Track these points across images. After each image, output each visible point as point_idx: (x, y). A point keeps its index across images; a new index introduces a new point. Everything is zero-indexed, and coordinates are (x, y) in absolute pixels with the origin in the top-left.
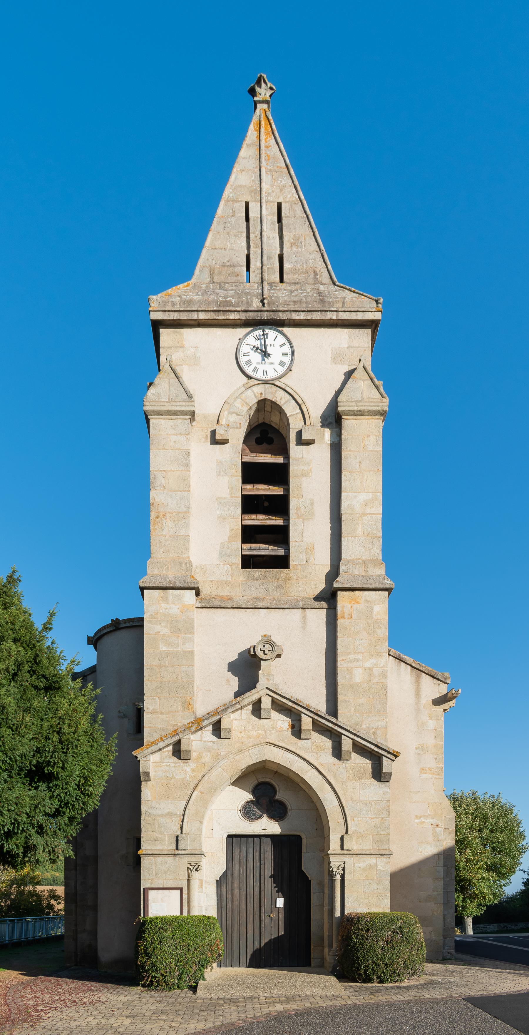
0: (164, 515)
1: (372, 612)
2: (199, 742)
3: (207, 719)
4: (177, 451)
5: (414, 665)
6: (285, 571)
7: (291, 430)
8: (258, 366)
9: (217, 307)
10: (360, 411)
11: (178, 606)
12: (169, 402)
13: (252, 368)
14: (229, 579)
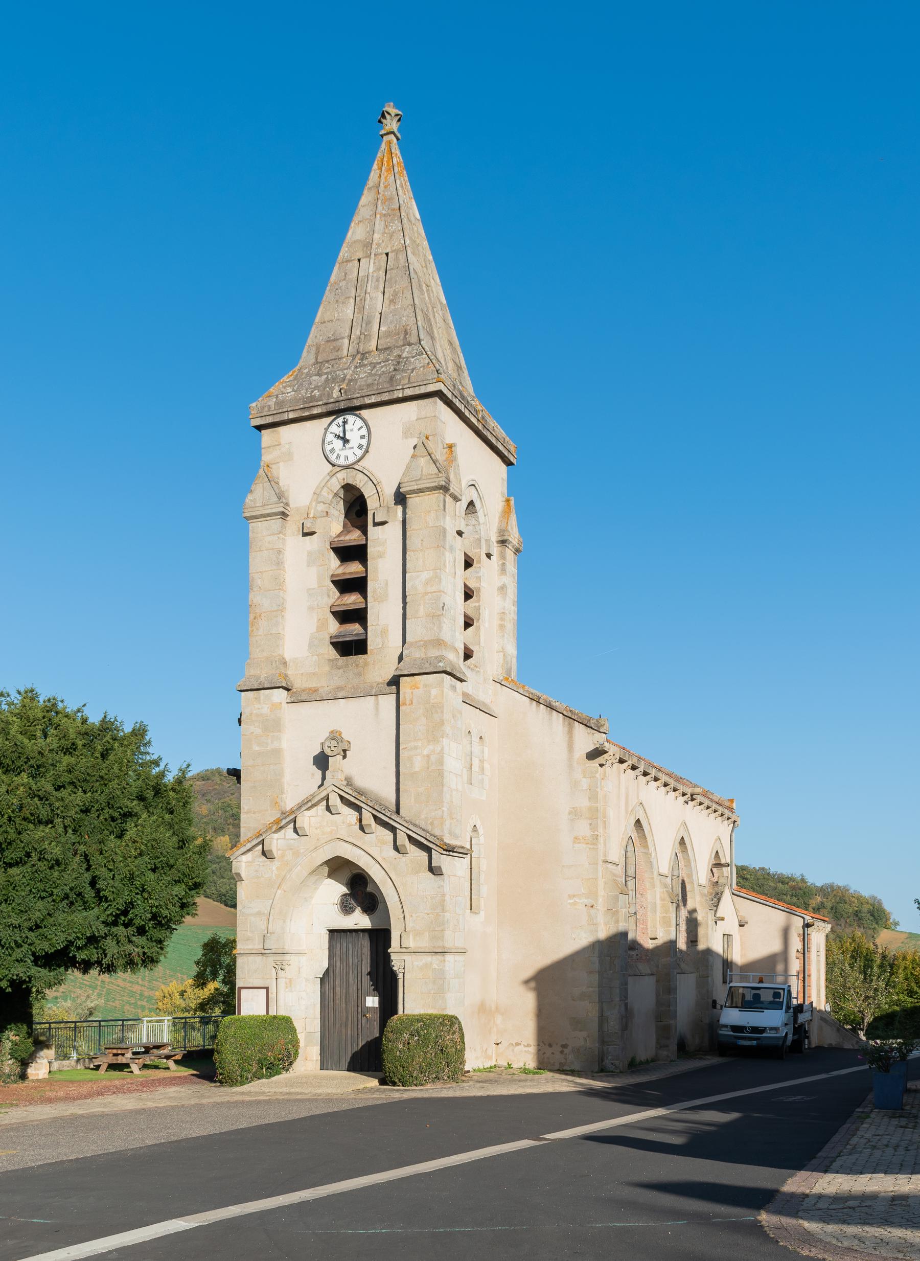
2: (278, 842)
3: (285, 818)
14: (317, 670)
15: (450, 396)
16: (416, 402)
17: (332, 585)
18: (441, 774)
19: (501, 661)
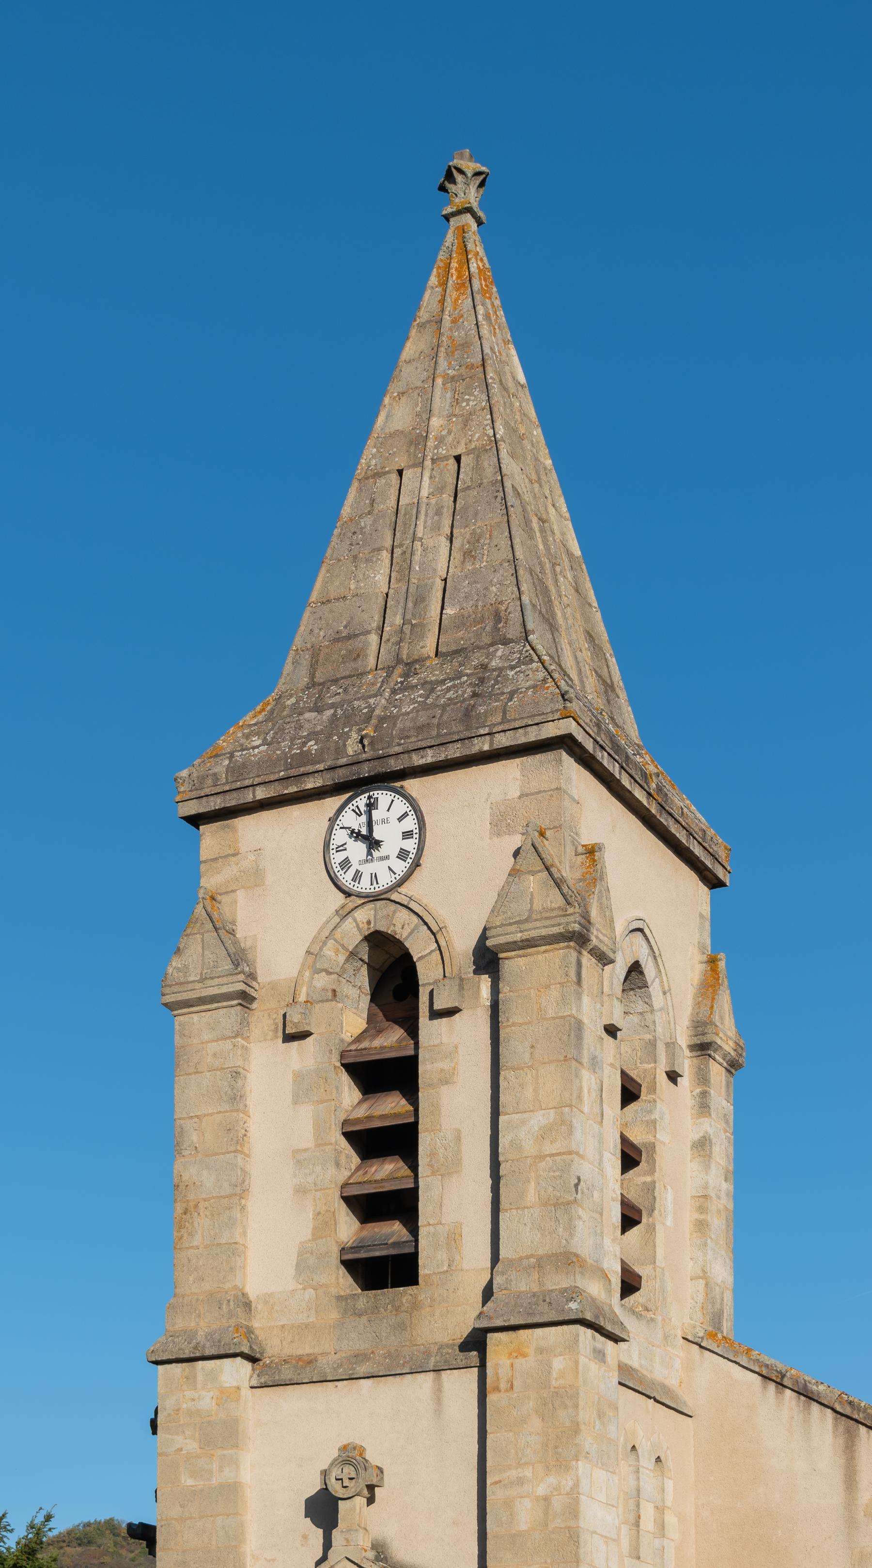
0: (196, 1206)
1: (549, 1373)
4: (218, 1073)
5: (838, 1408)
6: (411, 1290)
7: (421, 989)
8: (361, 868)
9: (286, 770)
10: (527, 940)
11: (212, 1393)
12: (202, 980)
13: (351, 873)
14: (312, 1319)
15: (589, 745)
16: (518, 761)
17: (344, 1143)
18: (573, 1536)
19: (701, 1297)
